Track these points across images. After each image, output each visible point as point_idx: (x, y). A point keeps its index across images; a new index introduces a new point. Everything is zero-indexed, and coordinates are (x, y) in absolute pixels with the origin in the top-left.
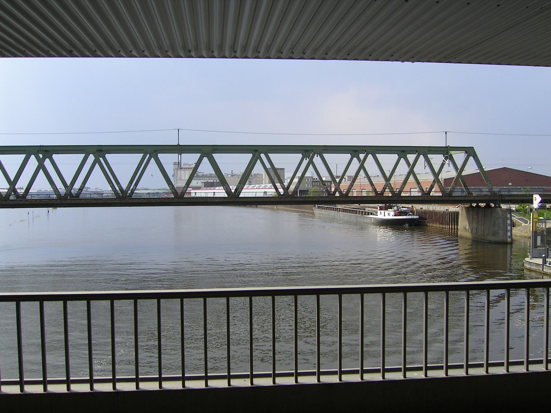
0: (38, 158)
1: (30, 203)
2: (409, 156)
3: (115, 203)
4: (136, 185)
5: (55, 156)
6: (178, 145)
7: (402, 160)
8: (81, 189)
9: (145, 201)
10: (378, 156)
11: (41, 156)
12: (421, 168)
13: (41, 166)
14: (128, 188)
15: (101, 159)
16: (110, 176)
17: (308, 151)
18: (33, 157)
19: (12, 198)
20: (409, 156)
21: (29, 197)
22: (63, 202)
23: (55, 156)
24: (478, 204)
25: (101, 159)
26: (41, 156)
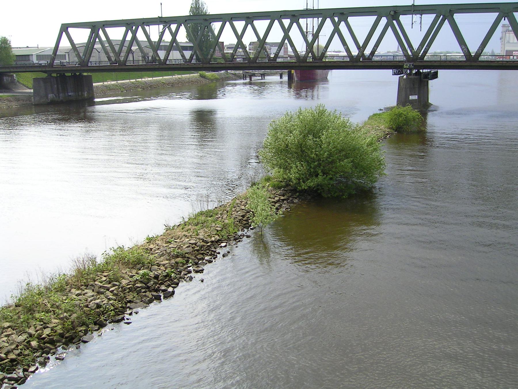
0: (333, 21)
1: (501, 65)
2: (236, 23)
3: (334, 66)
4: (429, 46)
5: (255, 22)
6: (413, 5)
7: (295, 25)
8: (373, 53)
9: (376, 64)
10: (106, 29)
11: (336, 19)
12: (295, 34)
13: (336, 30)
14: (420, 49)
15: (395, 22)
16: (402, 38)
17: (131, 25)
18: (328, 21)
19: (193, 61)
20: (236, 23)
21: (482, 58)
22: (355, 64)
23: (350, 19)
24: (418, 71)
25: (395, 22)
26: (336, 19)
